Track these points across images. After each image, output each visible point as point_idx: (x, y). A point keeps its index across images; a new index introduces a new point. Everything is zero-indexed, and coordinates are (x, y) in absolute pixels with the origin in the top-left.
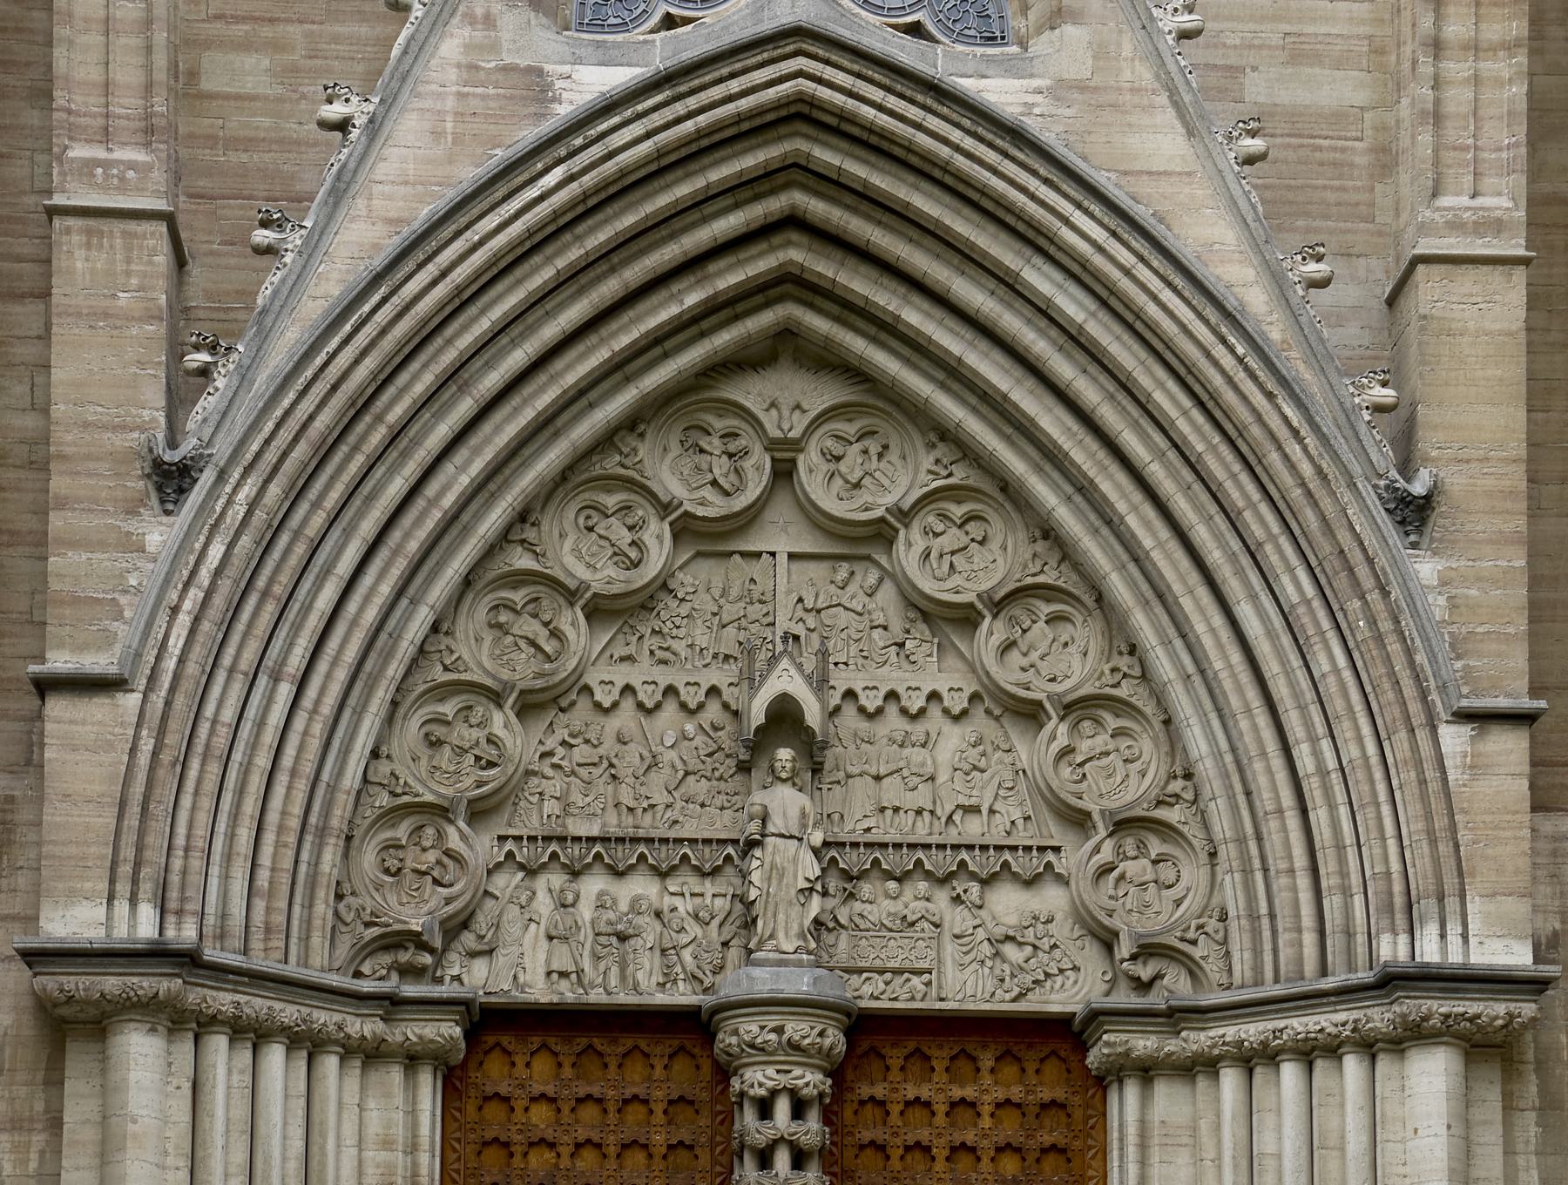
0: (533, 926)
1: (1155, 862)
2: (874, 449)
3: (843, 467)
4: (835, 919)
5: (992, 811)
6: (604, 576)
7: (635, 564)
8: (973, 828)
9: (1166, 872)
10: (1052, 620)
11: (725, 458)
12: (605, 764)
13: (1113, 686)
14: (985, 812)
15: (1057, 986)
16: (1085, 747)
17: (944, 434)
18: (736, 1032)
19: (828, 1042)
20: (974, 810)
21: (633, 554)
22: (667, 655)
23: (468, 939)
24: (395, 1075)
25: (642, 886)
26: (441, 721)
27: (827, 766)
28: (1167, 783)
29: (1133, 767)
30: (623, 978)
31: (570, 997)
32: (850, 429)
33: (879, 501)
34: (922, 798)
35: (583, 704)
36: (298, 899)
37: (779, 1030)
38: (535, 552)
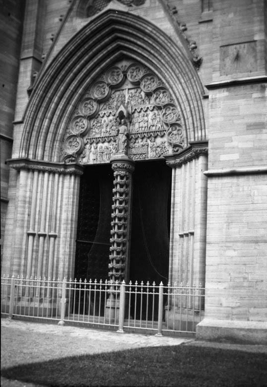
2: (138, 70)
6: (88, 113)
10: (163, 93)
17: (145, 67)
19: (125, 166)
20: (153, 126)
23: (82, 155)
24: (68, 177)
25: (106, 144)
26: (78, 122)
29: (175, 115)
30: (102, 159)
31: (95, 163)
33: (138, 78)
35: (99, 117)
36: (149, 49)
37: (124, 165)
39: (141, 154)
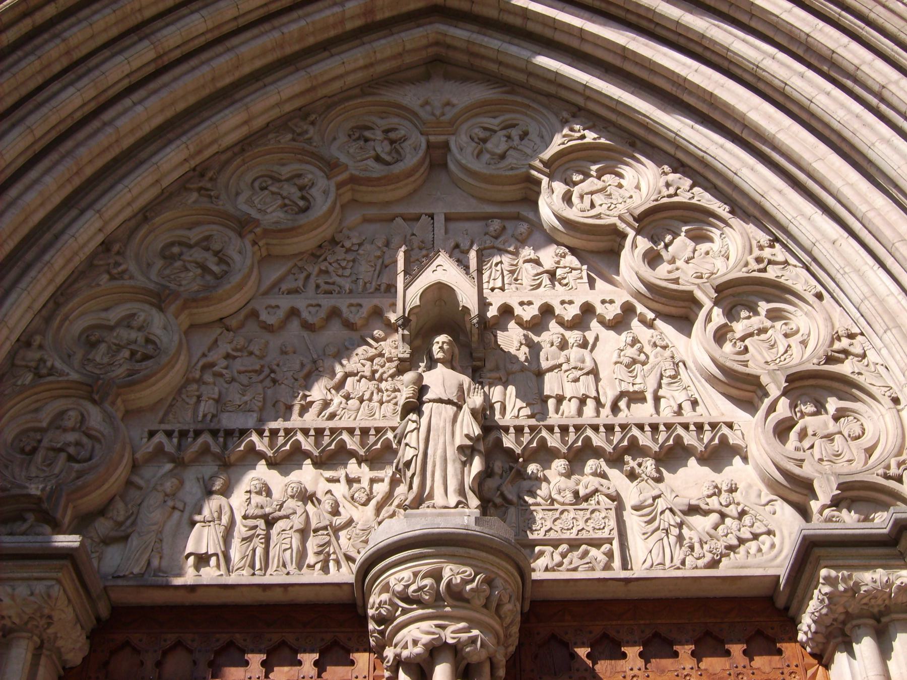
0: (177, 514)
1: (836, 418)
3: (489, 145)
4: (503, 496)
5: (657, 399)
7: (305, 210)
8: (643, 412)
9: (848, 426)
11: (386, 143)
12: (267, 371)
13: (760, 271)
14: (649, 396)
15: (753, 550)
16: (740, 327)
18: (386, 588)
20: (637, 397)
21: (301, 203)
22: (331, 287)
27: (489, 365)
28: (832, 343)
32: (494, 123)
34: (586, 386)
38: (210, 197)
39: (574, 545)
